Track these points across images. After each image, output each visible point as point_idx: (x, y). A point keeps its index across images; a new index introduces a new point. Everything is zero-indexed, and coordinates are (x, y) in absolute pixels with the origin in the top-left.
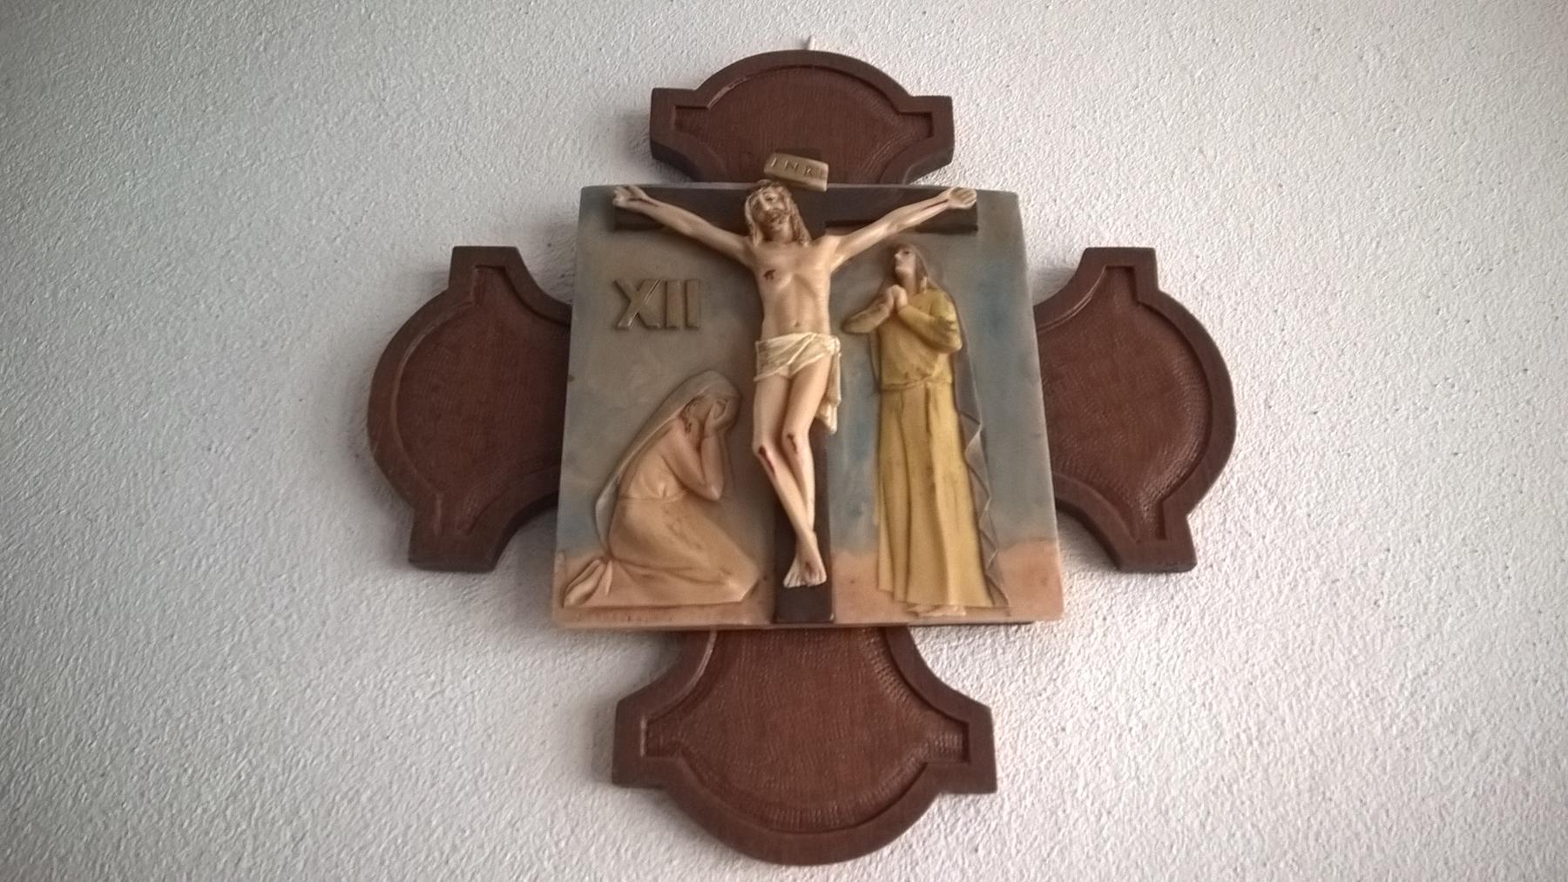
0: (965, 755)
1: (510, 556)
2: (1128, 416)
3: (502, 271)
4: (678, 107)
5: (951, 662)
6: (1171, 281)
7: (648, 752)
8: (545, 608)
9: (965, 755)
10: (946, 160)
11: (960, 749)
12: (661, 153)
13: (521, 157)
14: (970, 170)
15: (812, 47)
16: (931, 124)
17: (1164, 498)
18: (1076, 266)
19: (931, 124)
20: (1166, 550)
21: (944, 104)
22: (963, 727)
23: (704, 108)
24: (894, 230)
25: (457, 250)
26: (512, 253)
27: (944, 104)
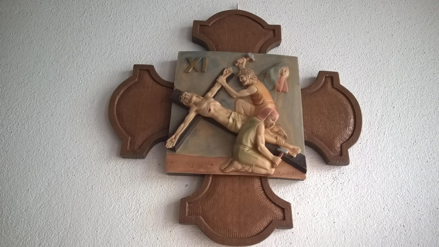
0: (284, 218)
1: (150, 155)
2: (331, 122)
3: (148, 71)
4: (200, 25)
5: (283, 192)
6: (344, 82)
7: (189, 213)
8: (167, 170)
9: (284, 218)
10: (278, 45)
11: (283, 217)
12: (195, 40)
13: (157, 44)
14: (284, 49)
15: (239, 8)
16: (274, 34)
17: (343, 144)
18: (316, 76)
19: (274, 34)
20: (342, 159)
21: (279, 27)
22: (283, 210)
23: (208, 26)
24: (241, 122)
25: (135, 65)
26: (152, 67)
27: (279, 27)
